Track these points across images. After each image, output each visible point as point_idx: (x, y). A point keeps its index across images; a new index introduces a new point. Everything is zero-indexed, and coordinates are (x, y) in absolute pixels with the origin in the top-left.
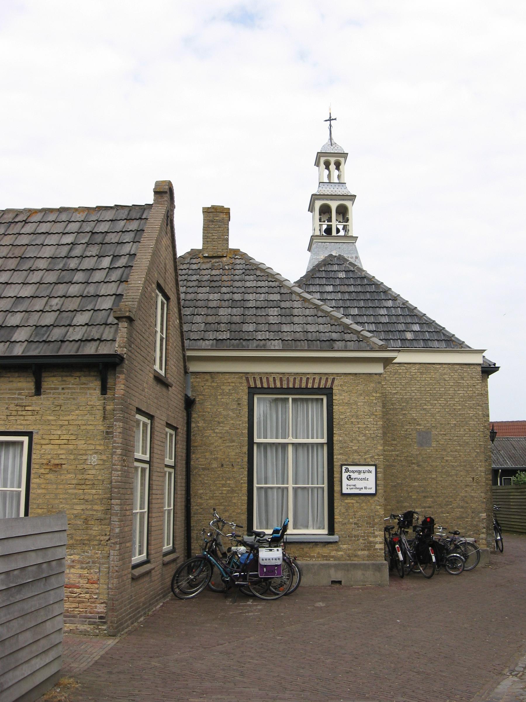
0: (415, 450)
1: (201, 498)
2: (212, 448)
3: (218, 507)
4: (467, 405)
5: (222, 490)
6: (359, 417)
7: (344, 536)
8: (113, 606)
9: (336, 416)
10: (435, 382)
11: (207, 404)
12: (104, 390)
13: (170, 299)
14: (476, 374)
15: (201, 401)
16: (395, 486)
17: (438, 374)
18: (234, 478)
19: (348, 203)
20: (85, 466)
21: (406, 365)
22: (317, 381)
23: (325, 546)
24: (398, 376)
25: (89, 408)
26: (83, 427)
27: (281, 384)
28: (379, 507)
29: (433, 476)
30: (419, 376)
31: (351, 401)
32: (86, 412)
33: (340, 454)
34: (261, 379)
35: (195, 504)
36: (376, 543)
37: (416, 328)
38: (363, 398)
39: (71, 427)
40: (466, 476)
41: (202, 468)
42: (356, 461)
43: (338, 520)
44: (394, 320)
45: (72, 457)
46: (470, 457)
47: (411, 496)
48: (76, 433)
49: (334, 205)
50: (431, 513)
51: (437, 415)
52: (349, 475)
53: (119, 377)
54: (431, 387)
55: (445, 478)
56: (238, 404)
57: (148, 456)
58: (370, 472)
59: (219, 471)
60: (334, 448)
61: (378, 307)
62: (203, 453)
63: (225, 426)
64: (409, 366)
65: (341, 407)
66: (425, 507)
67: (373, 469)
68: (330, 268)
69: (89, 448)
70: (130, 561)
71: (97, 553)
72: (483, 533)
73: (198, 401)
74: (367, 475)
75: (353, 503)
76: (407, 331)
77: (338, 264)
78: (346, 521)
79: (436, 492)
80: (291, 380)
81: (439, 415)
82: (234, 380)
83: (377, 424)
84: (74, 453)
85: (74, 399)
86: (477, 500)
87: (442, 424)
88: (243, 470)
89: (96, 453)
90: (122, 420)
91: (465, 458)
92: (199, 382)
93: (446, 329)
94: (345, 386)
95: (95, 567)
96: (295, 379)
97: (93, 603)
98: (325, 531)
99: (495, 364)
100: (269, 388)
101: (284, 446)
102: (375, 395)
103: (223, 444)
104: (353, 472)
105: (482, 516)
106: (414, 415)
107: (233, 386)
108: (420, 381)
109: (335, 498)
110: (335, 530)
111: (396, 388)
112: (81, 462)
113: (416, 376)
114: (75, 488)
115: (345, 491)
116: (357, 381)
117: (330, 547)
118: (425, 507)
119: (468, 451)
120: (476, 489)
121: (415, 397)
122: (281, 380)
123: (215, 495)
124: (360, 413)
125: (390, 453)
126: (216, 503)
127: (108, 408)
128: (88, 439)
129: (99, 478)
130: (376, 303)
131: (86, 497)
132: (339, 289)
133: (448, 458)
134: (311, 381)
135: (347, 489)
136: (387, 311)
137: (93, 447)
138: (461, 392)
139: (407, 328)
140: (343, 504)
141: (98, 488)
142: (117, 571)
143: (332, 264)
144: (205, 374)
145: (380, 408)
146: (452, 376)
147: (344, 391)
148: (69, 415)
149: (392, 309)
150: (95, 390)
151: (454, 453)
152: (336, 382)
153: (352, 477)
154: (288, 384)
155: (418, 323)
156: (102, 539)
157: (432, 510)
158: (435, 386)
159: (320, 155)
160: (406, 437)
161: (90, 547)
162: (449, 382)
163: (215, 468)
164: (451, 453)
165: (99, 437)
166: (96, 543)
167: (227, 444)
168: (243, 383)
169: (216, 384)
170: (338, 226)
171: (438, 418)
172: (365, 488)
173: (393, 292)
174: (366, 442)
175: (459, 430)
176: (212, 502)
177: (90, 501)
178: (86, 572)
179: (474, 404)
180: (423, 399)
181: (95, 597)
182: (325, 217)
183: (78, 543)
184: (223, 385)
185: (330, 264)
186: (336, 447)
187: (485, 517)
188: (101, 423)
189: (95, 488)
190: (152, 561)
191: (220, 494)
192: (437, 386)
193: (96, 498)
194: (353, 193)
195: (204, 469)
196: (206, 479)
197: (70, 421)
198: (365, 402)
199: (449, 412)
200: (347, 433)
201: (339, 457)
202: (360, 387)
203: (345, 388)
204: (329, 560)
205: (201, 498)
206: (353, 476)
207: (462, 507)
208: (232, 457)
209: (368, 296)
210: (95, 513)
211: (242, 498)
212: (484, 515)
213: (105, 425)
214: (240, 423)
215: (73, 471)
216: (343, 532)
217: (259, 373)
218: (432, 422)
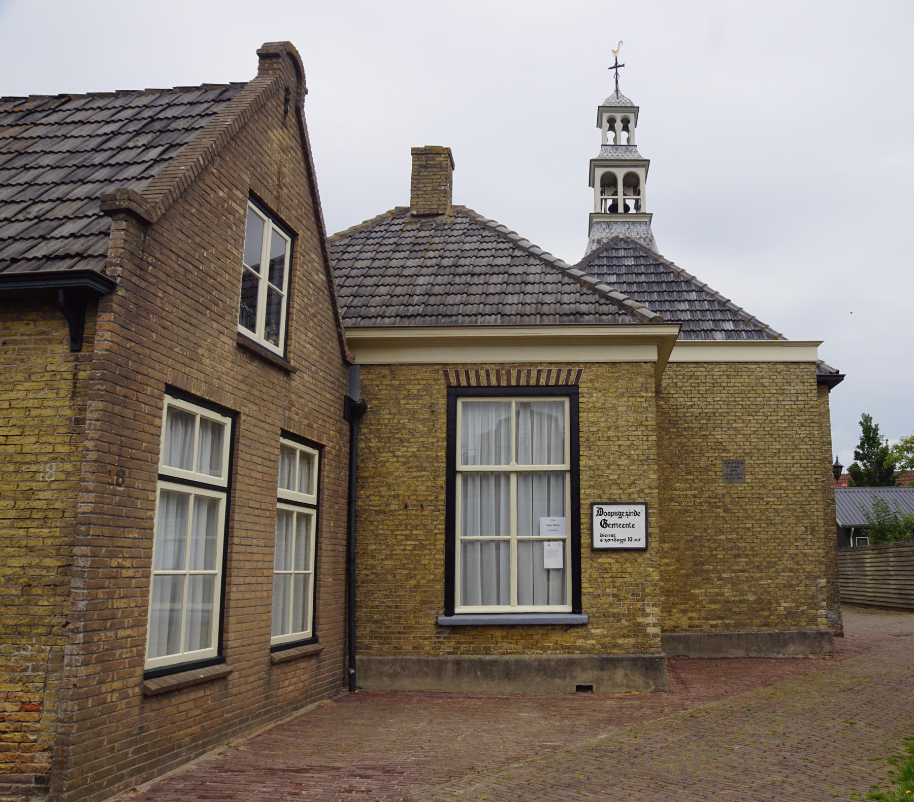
0: (720, 487)
1: (373, 557)
2: (390, 480)
3: (399, 571)
4: (796, 421)
5: (406, 545)
6: (620, 429)
7: (597, 615)
8: (62, 756)
9: (583, 428)
10: (749, 388)
11: (385, 413)
12: (78, 340)
13: (298, 235)
14: (809, 377)
15: (375, 408)
16: (692, 541)
17: (752, 377)
18: (425, 525)
19: (640, 172)
20: (34, 485)
21: (705, 365)
22: (554, 374)
23: (566, 630)
24: (695, 381)
25: (47, 377)
26: (34, 413)
27: (498, 380)
28: (651, 569)
29: (748, 526)
30: (726, 381)
31: (608, 405)
32: (42, 385)
33: (590, 487)
34: (467, 373)
35: (364, 567)
36: (648, 625)
37: (730, 326)
38: (626, 400)
39: (14, 413)
40: (796, 524)
41: (375, 511)
42: (615, 497)
43: (587, 590)
44: (699, 315)
45: (11, 468)
46: (802, 496)
47: (716, 555)
48: (22, 423)
49: (620, 173)
50: (745, 579)
51: (752, 436)
52: (604, 520)
53: (100, 316)
54: (744, 395)
55: (765, 528)
56: (432, 412)
57: (315, 496)
58: (636, 514)
59: (400, 515)
60: (581, 477)
61: (676, 300)
62: (377, 487)
63: (410, 447)
64: (710, 366)
65: (591, 415)
66: (736, 571)
67: (641, 509)
68: (614, 254)
69: (43, 451)
70: (141, 663)
71: (43, 651)
72: (822, 608)
73: (371, 408)
74: (632, 519)
75: (610, 564)
76: (716, 331)
77: (625, 249)
78: (599, 592)
79: (752, 548)
80: (514, 373)
81: (755, 436)
82: (426, 376)
83: (647, 440)
84: (15, 460)
85: (22, 361)
86: (813, 559)
87: (759, 450)
88: (438, 513)
89: (54, 459)
90: (102, 396)
91: (795, 499)
92: (372, 380)
93: (770, 327)
94: (598, 381)
95: (38, 678)
96: (519, 372)
97: (28, 750)
98: (568, 608)
99: (838, 372)
100: (479, 387)
101: (507, 474)
102: (644, 394)
103: (408, 474)
104: (610, 514)
105: (820, 583)
106: (719, 437)
107: (424, 385)
108: (727, 388)
109: (582, 556)
110: (583, 606)
111: (691, 398)
112: (27, 476)
113: (720, 381)
114: (11, 527)
115: (597, 544)
116: (616, 375)
117: (573, 632)
118: (736, 571)
119: (799, 488)
120: (812, 544)
121: (720, 411)
122: (498, 373)
123: (393, 552)
124: (622, 422)
125: (685, 493)
126: (396, 566)
127: (82, 375)
128: (43, 433)
129: (58, 505)
130: (675, 296)
131: (31, 543)
132: (624, 278)
133: (769, 499)
134: (544, 375)
135: (601, 541)
136: (690, 305)
137: (50, 449)
138: (787, 403)
139: (716, 327)
140: (595, 565)
141: (53, 525)
142: (75, 686)
143: (617, 249)
144: (382, 367)
145: (652, 415)
146: (773, 379)
147: (596, 389)
148: (12, 391)
149: (696, 302)
150: (61, 343)
151: (777, 492)
152: (583, 376)
153: (608, 523)
154: (509, 380)
155: (731, 320)
156: (55, 623)
157: (747, 574)
158: (749, 395)
159: (602, 109)
160: (706, 470)
161: (30, 638)
162: (769, 388)
163: (395, 510)
164: (774, 492)
165: (62, 430)
166: (41, 630)
167: (415, 474)
168: (439, 380)
169: (398, 382)
170: (627, 202)
171: (754, 440)
172: (630, 539)
173: (698, 281)
174: (631, 468)
175: (784, 458)
176: (389, 563)
177: (38, 550)
178: (20, 689)
179: (806, 420)
180: (732, 414)
181: (32, 738)
182: (609, 191)
183: (9, 631)
184: (409, 384)
185: (614, 248)
186: (584, 476)
187: (825, 585)
188: (67, 403)
189: (49, 524)
190: (228, 659)
191: (402, 550)
192: (752, 395)
193: (49, 544)
194: (645, 157)
195: (377, 513)
196: (380, 527)
197: (12, 402)
198: (629, 406)
199: (770, 432)
200: (601, 454)
201: (588, 491)
202: (621, 383)
203: (597, 385)
204: (573, 653)
205: (373, 557)
206: (611, 520)
207: (791, 570)
208: (421, 493)
209: (664, 287)
210: (44, 573)
211: (437, 556)
212: (823, 582)
213: (74, 407)
214: (435, 440)
215: (11, 494)
216: (595, 609)
217: (465, 364)
218: (745, 447)
